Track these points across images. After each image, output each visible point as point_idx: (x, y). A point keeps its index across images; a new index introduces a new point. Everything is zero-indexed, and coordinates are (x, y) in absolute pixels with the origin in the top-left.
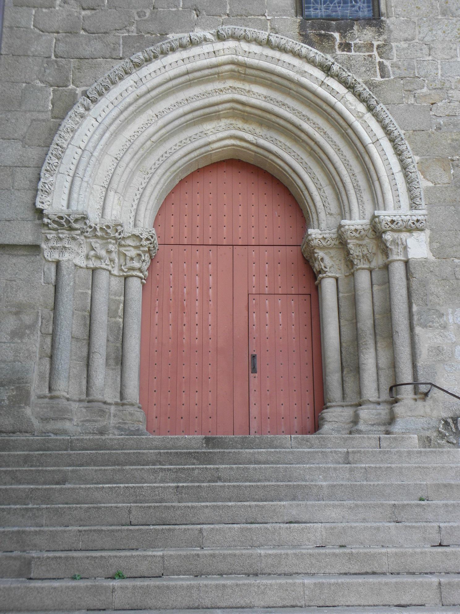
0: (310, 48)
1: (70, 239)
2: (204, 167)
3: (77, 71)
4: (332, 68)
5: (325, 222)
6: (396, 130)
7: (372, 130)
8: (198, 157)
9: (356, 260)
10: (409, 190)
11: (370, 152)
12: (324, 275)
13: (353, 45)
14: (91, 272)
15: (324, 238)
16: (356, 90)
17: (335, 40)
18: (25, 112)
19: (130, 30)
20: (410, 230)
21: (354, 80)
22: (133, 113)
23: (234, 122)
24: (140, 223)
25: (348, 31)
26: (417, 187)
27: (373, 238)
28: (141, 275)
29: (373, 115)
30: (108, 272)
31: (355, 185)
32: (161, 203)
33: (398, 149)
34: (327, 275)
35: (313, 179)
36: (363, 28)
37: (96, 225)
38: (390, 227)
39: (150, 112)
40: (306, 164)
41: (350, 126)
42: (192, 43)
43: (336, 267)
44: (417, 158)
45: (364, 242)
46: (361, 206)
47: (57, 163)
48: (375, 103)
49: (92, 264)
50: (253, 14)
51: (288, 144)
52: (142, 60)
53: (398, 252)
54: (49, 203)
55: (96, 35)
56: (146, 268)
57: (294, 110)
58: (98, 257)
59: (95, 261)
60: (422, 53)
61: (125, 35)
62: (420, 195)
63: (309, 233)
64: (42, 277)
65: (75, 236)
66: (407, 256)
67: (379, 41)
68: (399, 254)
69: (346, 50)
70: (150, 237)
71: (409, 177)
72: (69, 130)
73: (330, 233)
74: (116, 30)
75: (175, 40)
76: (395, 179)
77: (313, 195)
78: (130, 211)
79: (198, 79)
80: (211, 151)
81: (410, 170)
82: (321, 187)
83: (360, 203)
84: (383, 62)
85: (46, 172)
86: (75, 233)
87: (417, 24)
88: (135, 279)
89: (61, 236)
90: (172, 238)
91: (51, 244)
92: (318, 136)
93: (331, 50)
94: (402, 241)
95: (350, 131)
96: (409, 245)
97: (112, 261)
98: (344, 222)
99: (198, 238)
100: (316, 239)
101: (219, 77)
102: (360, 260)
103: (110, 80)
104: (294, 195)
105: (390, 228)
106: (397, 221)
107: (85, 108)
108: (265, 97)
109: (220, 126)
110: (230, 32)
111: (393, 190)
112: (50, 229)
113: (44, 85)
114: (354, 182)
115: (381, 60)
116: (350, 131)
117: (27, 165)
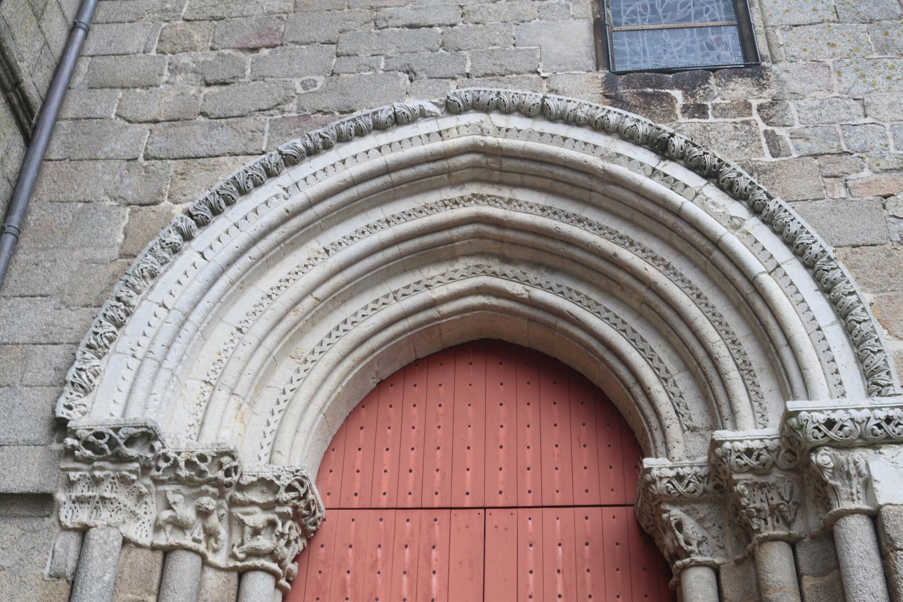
0: (625, 113)
1: (116, 481)
2: (428, 356)
3: (180, 177)
4: (670, 142)
5: (681, 445)
6: (814, 243)
7: (764, 249)
8: (413, 332)
9: (755, 520)
10: (860, 359)
11: (764, 289)
12: (687, 560)
13: (710, 107)
14: (159, 556)
15: (680, 478)
16: (724, 177)
17: (674, 101)
18: (73, 249)
19: (286, 109)
20: (873, 443)
21: (717, 159)
22: (279, 244)
23: (482, 262)
24: (279, 456)
25: (699, 86)
26: (876, 349)
27: (789, 470)
28: (274, 566)
29: (764, 222)
30: (197, 560)
31: (740, 362)
32: (338, 427)
33: (824, 280)
34: (692, 561)
35: (650, 362)
36: (727, 81)
37: (179, 454)
38: (825, 435)
39: (314, 246)
40: (634, 331)
41: (717, 243)
42: (397, 120)
43: (714, 542)
44: (868, 297)
45: (771, 479)
46: (756, 404)
47: (114, 332)
48: (765, 197)
49: (163, 540)
50: (515, 70)
51: (595, 296)
52: (301, 152)
53: (852, 494)
54: (83, 409)
55: (224, 120)
56: (289, 553)
57: (601, 229)
58: (180, 526)
59: (171, 533)
60: (850, 113)
61: (275, 117)
62: (886, 364)
63: (645, 466)
64: (48, 563)
65: (127, 473)
66: (876, 500)
67: (761, 98)
68: (855, 497)
69: (696, 115)
70: (297, 484)
71: (855, 332)
72: (146, 273)
73: (692, 466)
74: (260, 110)
75: (365, 115)
76: (824, 339)
77: (652, 390)
78: (262, 434)
79: (408, 182)
80: (438, 319)
81: (855, 318)
82: (669, 375)
83: (754, 398)
84: (773, 131)
85: (87, 349)
86: (126, 469)
87: (832, 68)
88: (260, 575)
89: (97, 473)
90: (356, 494)
91: (77, 492)
92: (654, 273)
93: (669, 114)
94: (857, 468)
95: (717, 255)
96: (875, 474)
97: (210, 534)
98: (719, 435)
99: (410, 494)
100: (661, 478)
101: (452, 178)
102: (765, 520)
103: (236, 187)
104: (614, 402)
105: (826, 440)
106: (840, 423)
107: (182, 234)
108: (543, 210)
109: (456, 271)
110: (470, 98)
111: (825, 363)
112: (76, 460)
113: (116, 204)
114: (737, 356)
115: (769, 128)
116: (717, 255)
117: (56, 341)
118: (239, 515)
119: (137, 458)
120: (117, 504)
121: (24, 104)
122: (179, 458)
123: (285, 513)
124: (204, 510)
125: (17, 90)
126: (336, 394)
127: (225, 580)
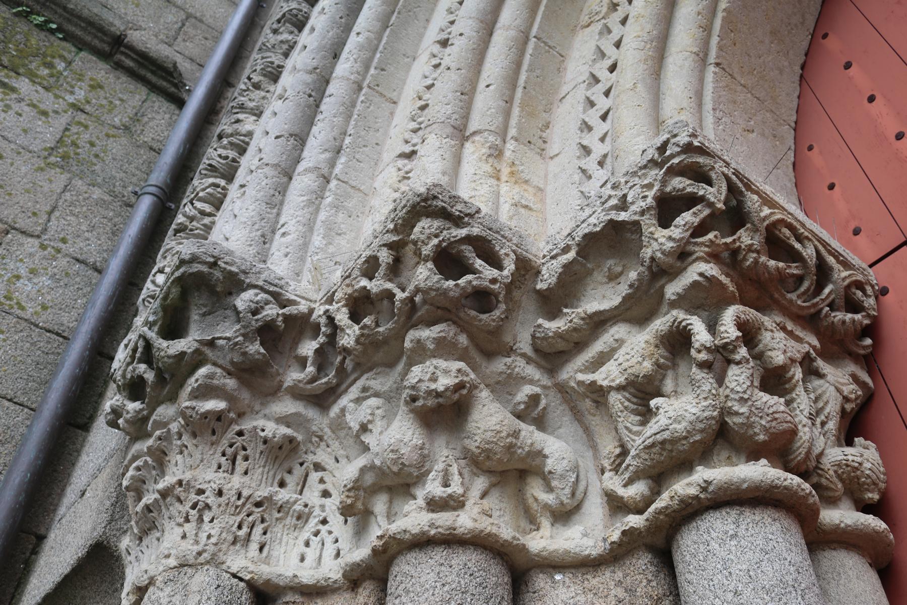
70: (679, 183)
118: (581, 377)
119: (197, 351)
120: (193, 497)
121: (146, 63)
122: (332, 308)
123: (695, 284)
124: (431, 402)
125: (122, 49)
126: (720, 15)
127: (620, 592)
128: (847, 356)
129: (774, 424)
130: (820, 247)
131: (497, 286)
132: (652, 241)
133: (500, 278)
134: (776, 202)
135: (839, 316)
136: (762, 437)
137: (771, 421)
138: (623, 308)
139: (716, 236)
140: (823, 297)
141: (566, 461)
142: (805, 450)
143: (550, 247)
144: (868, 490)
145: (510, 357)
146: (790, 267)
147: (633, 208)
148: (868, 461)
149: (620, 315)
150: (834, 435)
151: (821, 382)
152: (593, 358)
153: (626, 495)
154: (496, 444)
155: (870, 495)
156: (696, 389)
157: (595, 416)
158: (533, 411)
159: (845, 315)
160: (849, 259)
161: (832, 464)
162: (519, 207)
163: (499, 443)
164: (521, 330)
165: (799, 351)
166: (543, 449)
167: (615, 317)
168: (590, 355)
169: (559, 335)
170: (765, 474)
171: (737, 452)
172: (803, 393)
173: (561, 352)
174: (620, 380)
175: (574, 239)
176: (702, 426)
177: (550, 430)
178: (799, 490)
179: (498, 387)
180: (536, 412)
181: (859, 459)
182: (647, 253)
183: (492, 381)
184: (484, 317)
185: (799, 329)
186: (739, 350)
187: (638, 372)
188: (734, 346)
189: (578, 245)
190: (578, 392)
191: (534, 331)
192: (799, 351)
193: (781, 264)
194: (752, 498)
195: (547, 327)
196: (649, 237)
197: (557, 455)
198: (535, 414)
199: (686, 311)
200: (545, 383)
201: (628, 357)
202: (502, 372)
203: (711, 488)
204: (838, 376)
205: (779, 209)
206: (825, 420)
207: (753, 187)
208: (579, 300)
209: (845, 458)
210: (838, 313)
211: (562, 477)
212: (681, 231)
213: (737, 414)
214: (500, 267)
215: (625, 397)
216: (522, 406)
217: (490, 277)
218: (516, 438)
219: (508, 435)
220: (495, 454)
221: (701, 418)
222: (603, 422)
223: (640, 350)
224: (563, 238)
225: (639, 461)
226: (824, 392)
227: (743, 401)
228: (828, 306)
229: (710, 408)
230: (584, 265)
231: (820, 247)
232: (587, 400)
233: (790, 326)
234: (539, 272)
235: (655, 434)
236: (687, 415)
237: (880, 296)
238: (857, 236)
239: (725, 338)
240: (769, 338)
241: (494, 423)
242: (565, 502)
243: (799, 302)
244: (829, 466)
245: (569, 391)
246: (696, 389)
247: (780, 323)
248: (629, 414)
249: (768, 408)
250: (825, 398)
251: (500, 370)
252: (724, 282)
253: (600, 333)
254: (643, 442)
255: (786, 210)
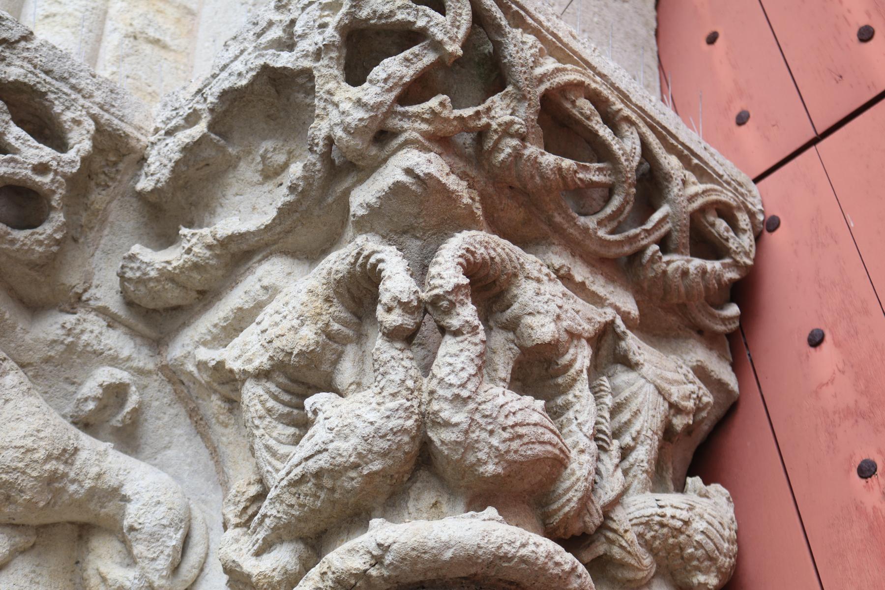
123: (397, 189)
128: (695, 335)
129: (515, 445)
130: (652, 139)
131: (47, 179)
132: (330, 108)
133: (54, 163)
134: (575, 53)
135: (677, 262)
136: (490, 469)
137: (511, 440)
138: (278, 229)
139: (442, 104)
140: (649, 226)
141: (163, 509)
142: (579, 495)
143: (168, 113)
144: (698, 569)
145: (75, 313)
146: (586, 169)
147: (304, 45)
148: (702, 517)
149: (275, 242)
150: (646, 471)
151: (631, 376)
152: (226, 319)
153: (255, 572)
154: (24, 473)
155: (701, 578)
156: (380, 377)
157: (226, 426)
158: (114, 415)
159: (688, 261)
160: (712, 163)
161: (634, 521)
162: (140, 40)
163: (28, 471)
164: (103, 265)
165: (589, 320)
166: (121, 485)
167: (267, 245)
168: (222, 314)
169: (168, 276)
170: (486, 534)
171: (451, 494)
172: (587, 393)
173: (177, 309)
174: (261, 360)
175: (205, 99)
176: (385, 445)
177: (148, 451)
178: (550, 564)
179: (48, 368)
180: (120, 417)
181: (685, 515)
182: (320, 129)
183: (36, 357)
184: (20, 235)
185: (601, 280)
186: (459, 309)
187: (290, 346)
188: (450, 301)
189: (211, 110)
190: (200, 383)
191: (123, 267)
192: (589, 320)
193: (567, 163)
194: (464, 578)
195: (146, 260)
196: (326, 100)
197: (146, 497)
198: (117, 421)
199: (384, 237)
200: (141, 364)
201: (277, 318)
202: (54, 341)
203: (388, 559)
204: (665, 368)
205: (577, 64)
206: (632, 444)
207: (530, 20)
208: (213, 213)
209: (659, 511)
210: (674, 257)
211: (154, 537)
212: (378, 90)
213: (447, 424)
214: (61, 145)
215: (268, 392)
216: (91, 406)
217: (35, 161)
218: (66, 462)
219: (49, 458)
220: (21, 491)
221: (383, 431)
222: (240, 439)
223: (298, 306)
224: (189, 97)
225: (281, 509)
226: (634, 395)
227: (459, 401)
228: (656, 242)
229: (401, 413)
230: (221, 149)
231: (652, 139)
232: (214, 397)
233: (580, 273)
234: (143, 159)
235: (307, 459)
236: (360, 424)
237: (766, 233)
238: (743, 127)
239: (435, 287)
240: (530, 293)
241: (23, 434)
242: (156, 585)
243: (602, 233)
244: (627, 525)
245: (185, 381)
246: (380, 377)
247: (561, 267)
248: (274, 423)
249: (506, 416)
250: (634, 406)
251: (51, 337)
252: (453, 187)
253: (241, 275)
254: (288, 474)
255: (593, 68)
